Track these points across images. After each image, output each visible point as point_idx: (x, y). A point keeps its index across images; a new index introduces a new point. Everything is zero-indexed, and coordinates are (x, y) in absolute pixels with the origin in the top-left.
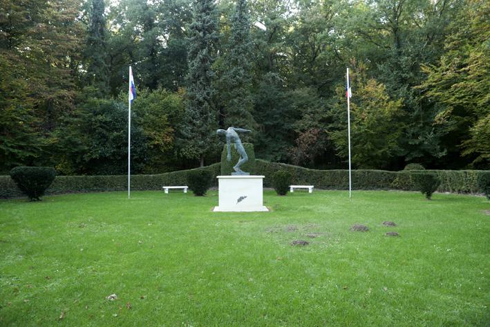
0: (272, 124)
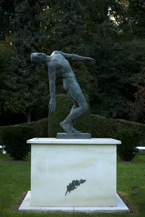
0: (107, 77)
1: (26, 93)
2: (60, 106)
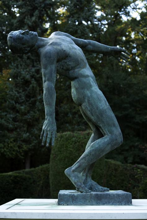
1: (23, 134)
2: (66, 148)
